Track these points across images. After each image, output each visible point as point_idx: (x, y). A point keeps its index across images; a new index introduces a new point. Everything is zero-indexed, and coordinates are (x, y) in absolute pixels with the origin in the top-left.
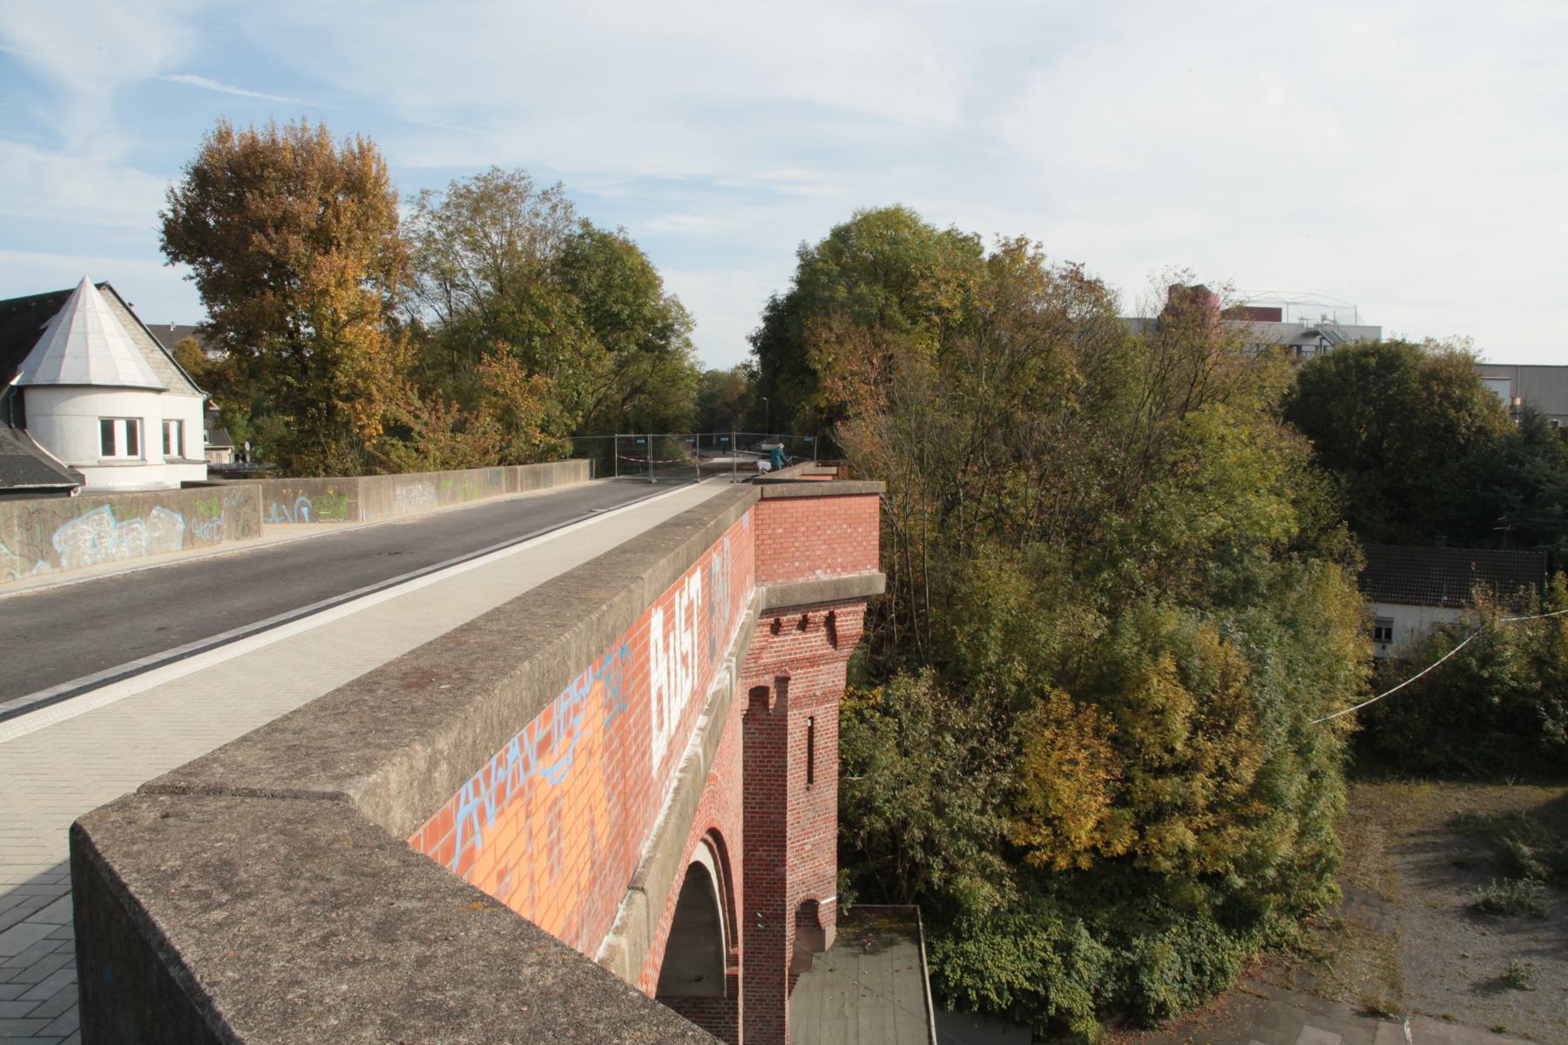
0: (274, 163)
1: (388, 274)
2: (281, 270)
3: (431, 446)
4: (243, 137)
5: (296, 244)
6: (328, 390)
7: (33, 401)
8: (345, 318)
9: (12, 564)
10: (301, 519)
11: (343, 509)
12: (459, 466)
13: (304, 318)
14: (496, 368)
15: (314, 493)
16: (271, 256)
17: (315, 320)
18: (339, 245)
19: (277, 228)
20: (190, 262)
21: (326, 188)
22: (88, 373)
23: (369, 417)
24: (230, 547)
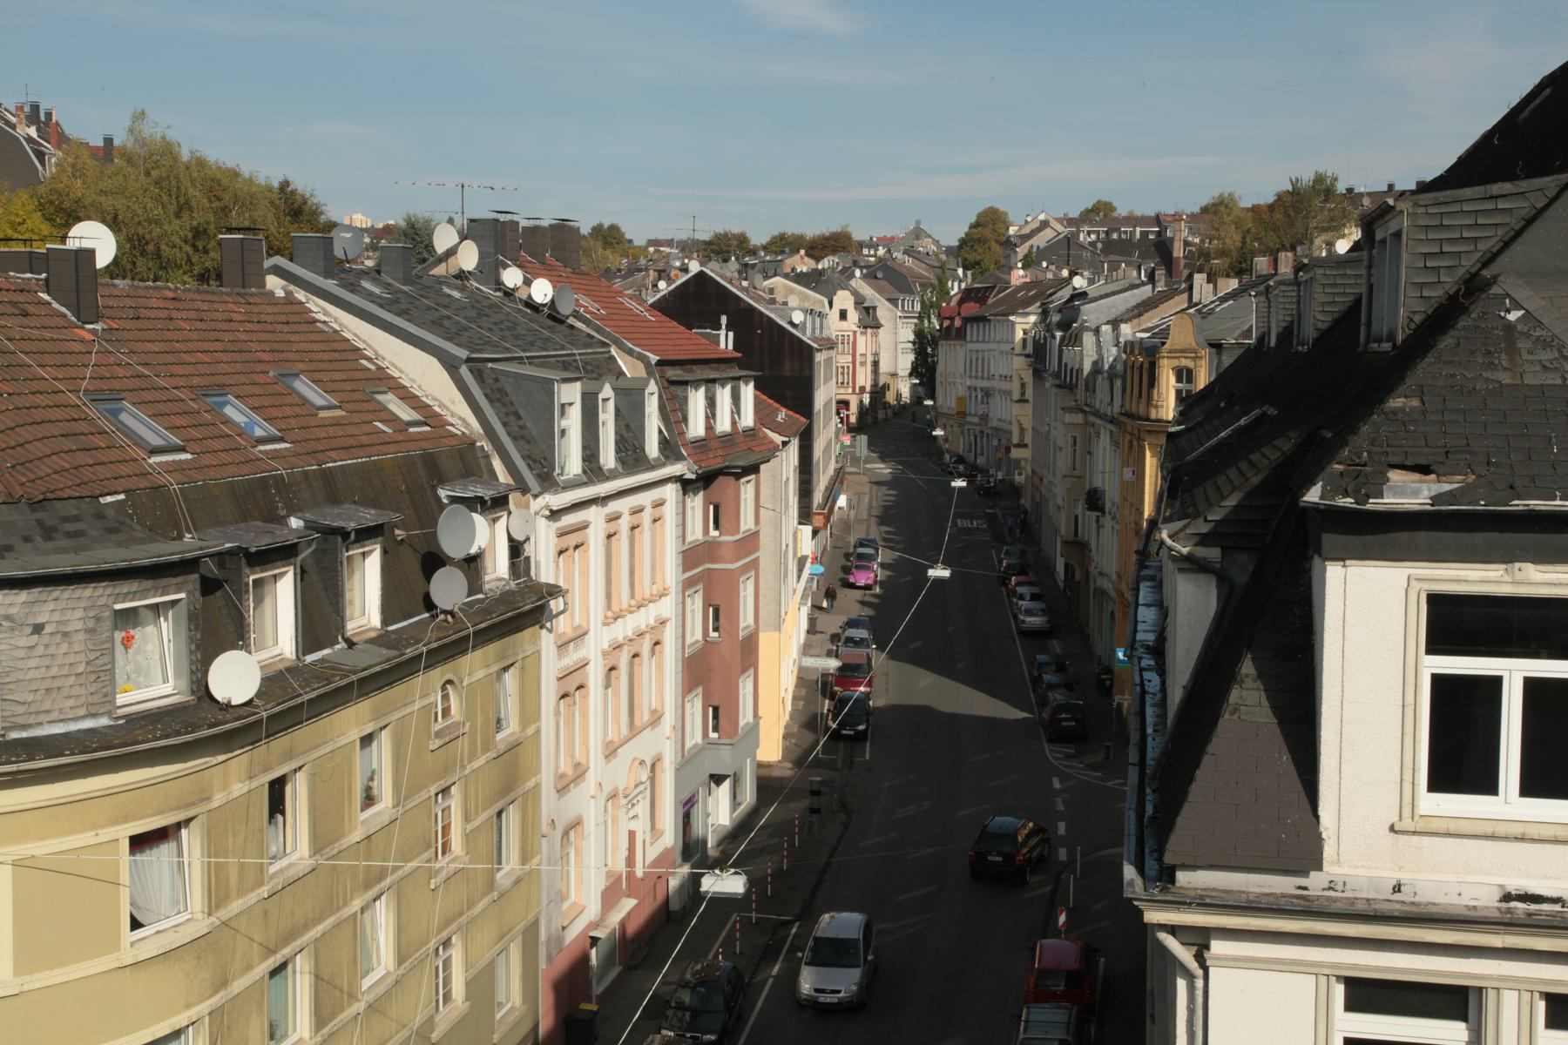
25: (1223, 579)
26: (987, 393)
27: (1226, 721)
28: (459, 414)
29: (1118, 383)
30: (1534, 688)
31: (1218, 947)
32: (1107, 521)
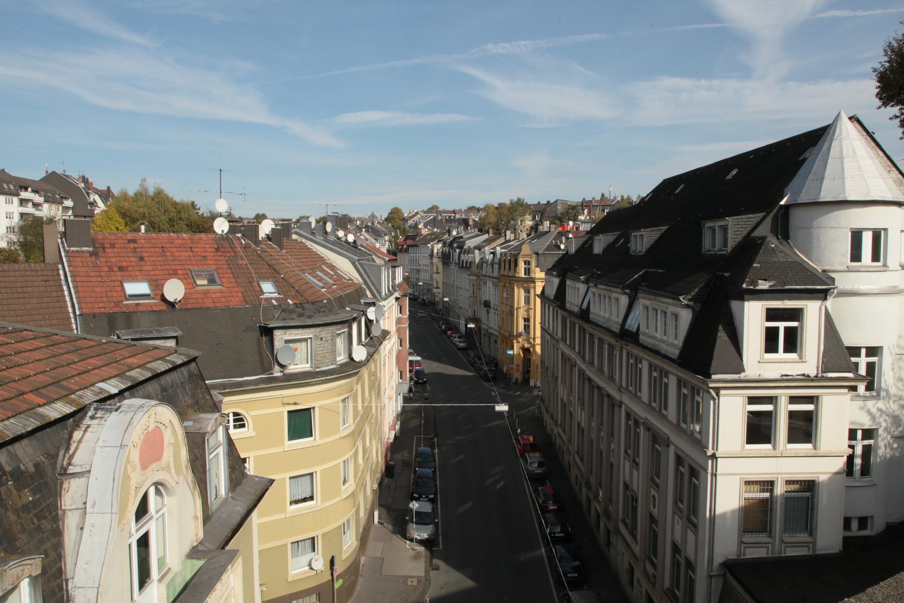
7: (796, 216)
22: (844, 191)
25: (693, 310)
26: (418, 271)
27: (718, 341)
29: (496, 266)
30: (786, 329)
31: (722, 392)
32: (492, 311)
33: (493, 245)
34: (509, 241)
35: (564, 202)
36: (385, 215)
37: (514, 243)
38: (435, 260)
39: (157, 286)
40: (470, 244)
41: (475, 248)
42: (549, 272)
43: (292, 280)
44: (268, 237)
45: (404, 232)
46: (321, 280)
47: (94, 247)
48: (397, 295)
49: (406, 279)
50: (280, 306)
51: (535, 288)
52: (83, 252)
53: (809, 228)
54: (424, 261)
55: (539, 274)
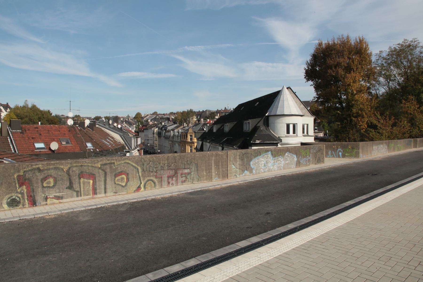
0: (334, 49)
1: (369, 78)
2: (337, 80)
3: (384, 131)
4: (325, 44)
5: (341, 72)
6: (350, 115)
7: (271, 119)
8: (355, 92)
9: (236, 172)
10: (339, 156)
11: (354, 153)
12: (394, 139)
13: (343, 93)
14: (408, 104)
15: (343, 147)
16: (333, 76)
17: (346, 94)
18: (354, 70)
19: (335, 67)
20: (312, 81)
21: (350, 54)
23: (362, 122)
24: (312, 167)
26: (148, 140)
28: (122, 141)
29: (179, 137)
33: (179, 129)
34: (185, 127)
35: (209, 111)
36: (134, 116)
37: (187, 128)
38: (155, 135)
39: (48, 145)
40: (169, 128)
41: (171, 130)
42: (198, 139)
43: (98, 142)
44: (88, 126)
45: (142, 123)
46: (109, 142)
47: (22, 130)
48: (138, 149)
49: (142, 143)
50: (94, 152)
51: (194, 145)
52: (18, 132)
53: (274, 123)
54: (151, 136)
55: (195, 140)
